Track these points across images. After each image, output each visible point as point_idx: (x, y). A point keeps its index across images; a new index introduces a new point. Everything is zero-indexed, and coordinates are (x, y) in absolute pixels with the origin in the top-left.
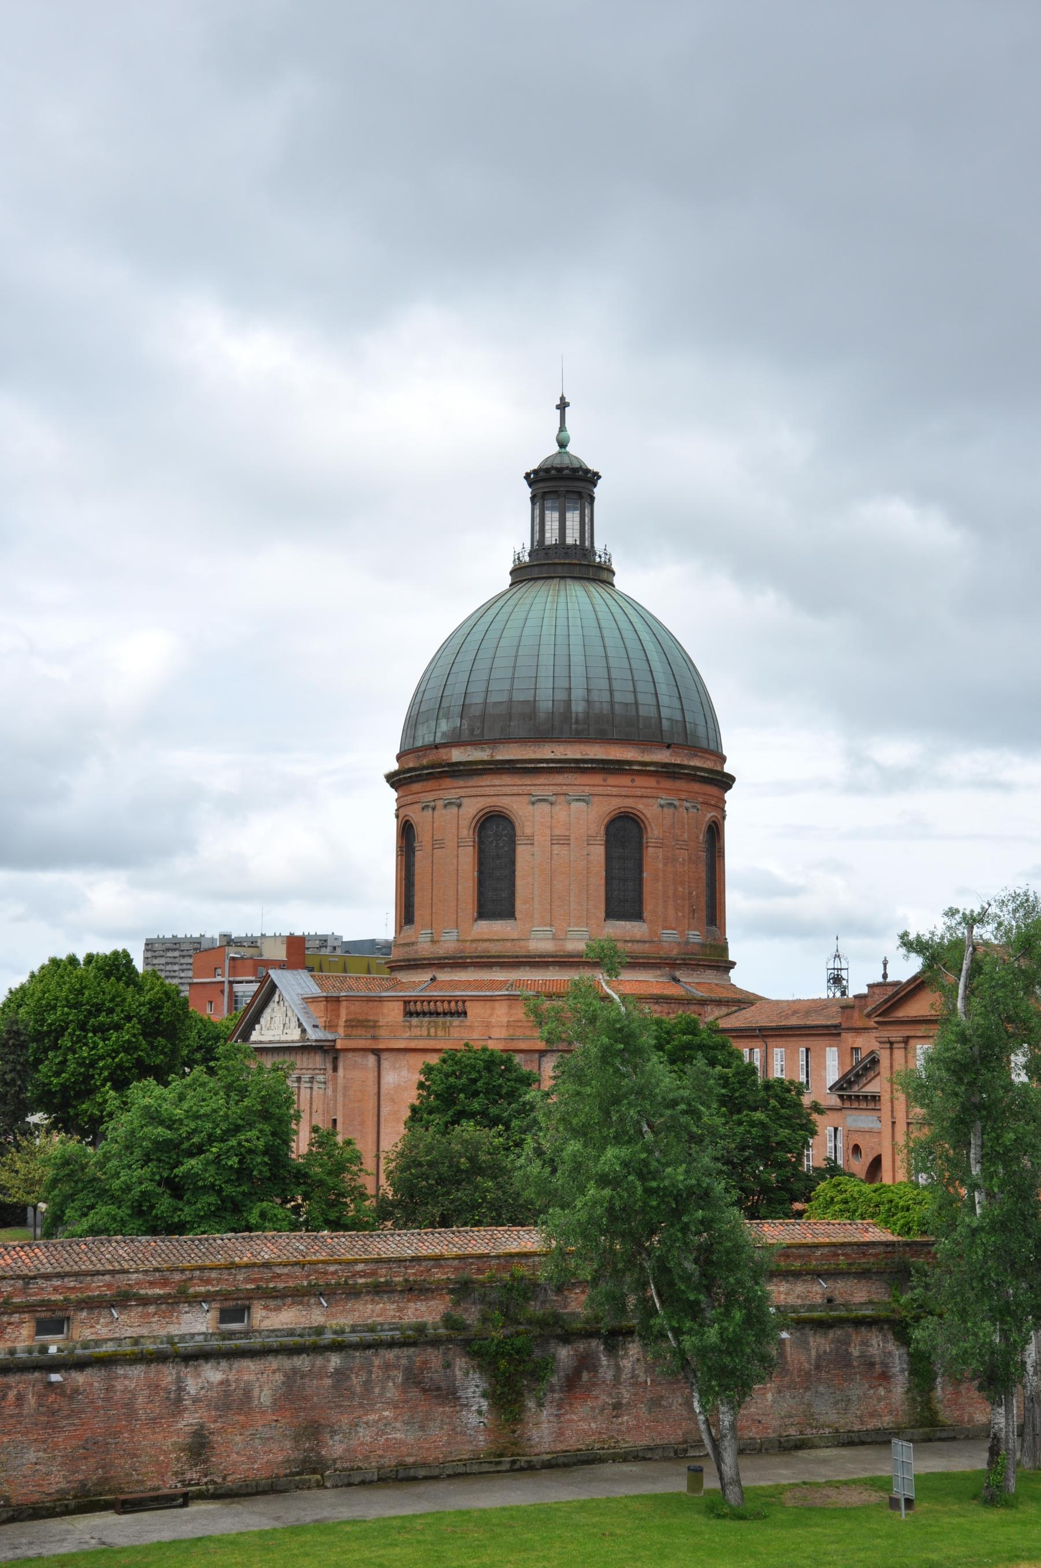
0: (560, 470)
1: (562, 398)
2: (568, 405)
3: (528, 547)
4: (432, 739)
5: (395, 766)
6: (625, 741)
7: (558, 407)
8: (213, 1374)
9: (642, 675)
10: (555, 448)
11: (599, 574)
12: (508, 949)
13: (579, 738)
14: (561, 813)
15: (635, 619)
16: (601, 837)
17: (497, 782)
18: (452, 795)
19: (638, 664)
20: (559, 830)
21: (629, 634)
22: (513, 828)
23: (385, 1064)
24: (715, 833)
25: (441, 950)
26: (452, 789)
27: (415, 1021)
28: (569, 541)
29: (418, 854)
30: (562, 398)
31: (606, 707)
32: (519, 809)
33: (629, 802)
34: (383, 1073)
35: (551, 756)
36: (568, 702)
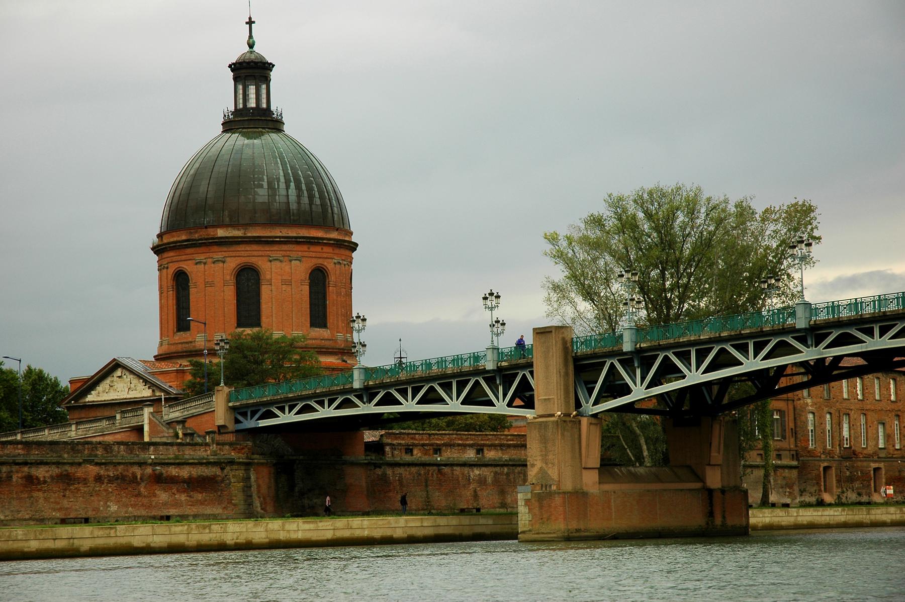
0: (248, 63)
1: (250, 18)
2: (254, 22)
7: (247, 23)
8: (477, 472)
10: (247, 49)
11: (276, 125)
14: (286, 266)
16: (308, 281)
18: (218, 256)
26: (218, 254)
30: (250, 18)
32: (263, 264)
33: (320, 261)
35: (280, 234)
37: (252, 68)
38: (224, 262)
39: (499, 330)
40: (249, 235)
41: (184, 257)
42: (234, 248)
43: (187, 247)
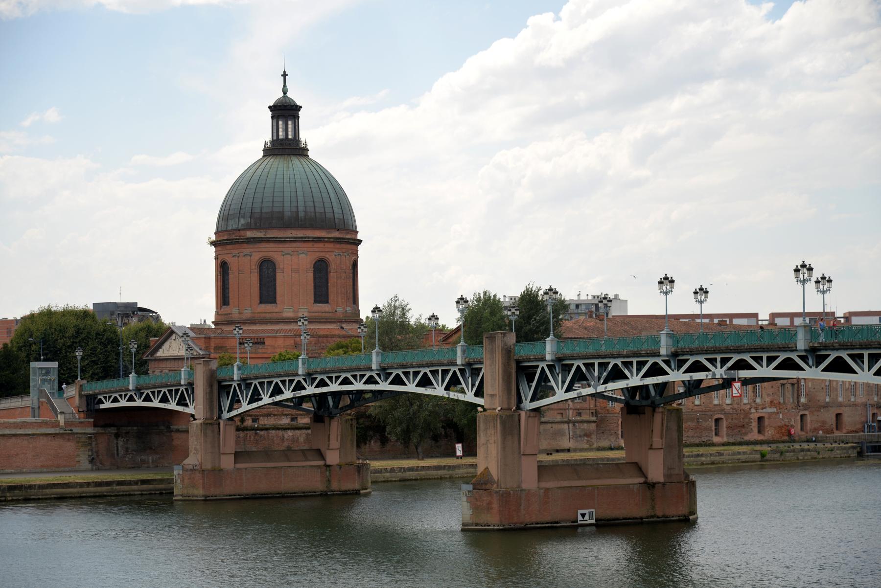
0: (286, 106)
5: (214, 238)
6: (321, 228)
9: (326, 200)
10: (282, 94)
12: (275, 316)
13: (303, 226)
15: (322, 174)
18: (247, 251)
19: (325, 195)
20: (294, 266)
21: (320, 181)
22: (274, 265)
24: (355, 265)
25: (244, 317)
26: (247, 249)
28: (290, 137)
29: (231, 276)
31: (313, 214)
32: (277, 257)
36: (297, 212)
39: (826, 287)
41: (226, 252)
42: (258, 245)
43: (227, 244)
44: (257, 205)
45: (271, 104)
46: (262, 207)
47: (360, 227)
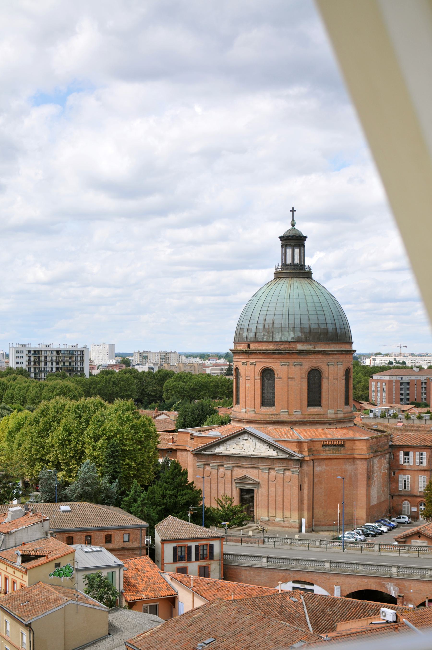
1: (293, 208)
3: (280, 265)
4: (287, 339)
10: (290, 227)
17: (317, 357)
23: (316, 464)
26: (298, 360)
27: (327, 448)
30: (293, 208)
34: (315, 467)
35: (333, 349)
37: (290, 239)
38: (301, 365)
40: (317, 349)
41: (271, 360)
43: (275, 354)
44: (305, 322)
45: (282, 235)
46: (310, 323)
47: (354, 339)
